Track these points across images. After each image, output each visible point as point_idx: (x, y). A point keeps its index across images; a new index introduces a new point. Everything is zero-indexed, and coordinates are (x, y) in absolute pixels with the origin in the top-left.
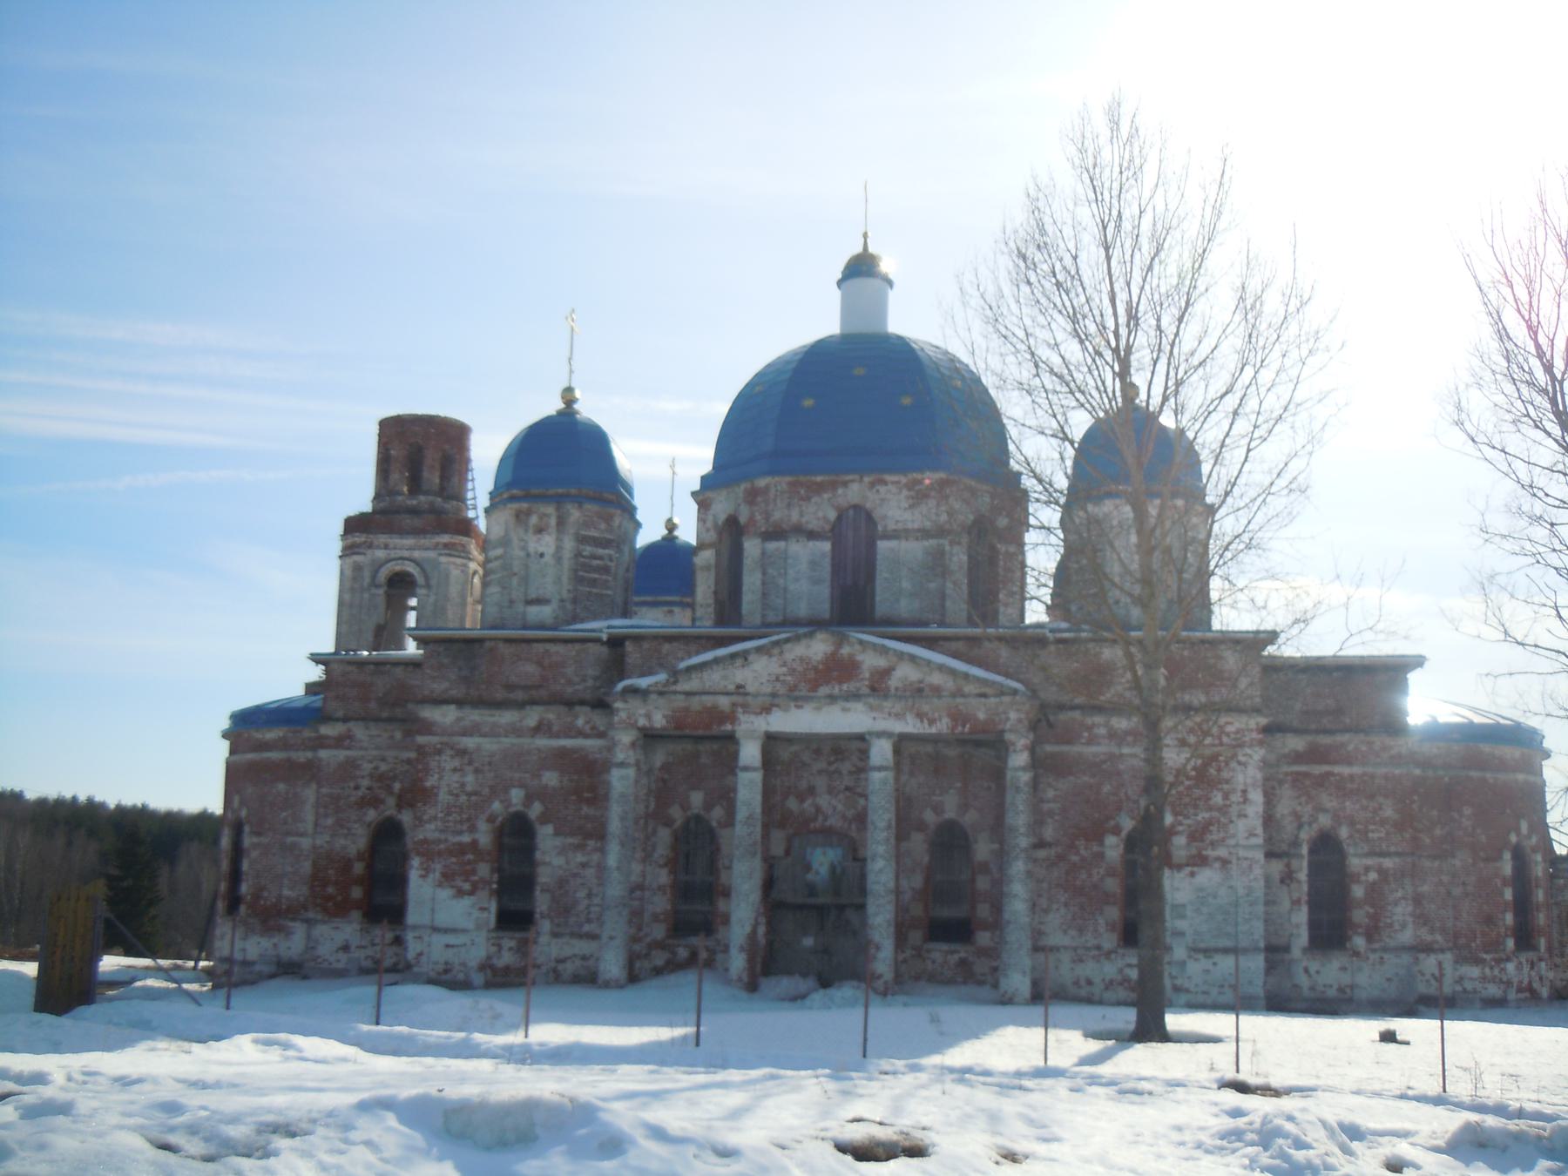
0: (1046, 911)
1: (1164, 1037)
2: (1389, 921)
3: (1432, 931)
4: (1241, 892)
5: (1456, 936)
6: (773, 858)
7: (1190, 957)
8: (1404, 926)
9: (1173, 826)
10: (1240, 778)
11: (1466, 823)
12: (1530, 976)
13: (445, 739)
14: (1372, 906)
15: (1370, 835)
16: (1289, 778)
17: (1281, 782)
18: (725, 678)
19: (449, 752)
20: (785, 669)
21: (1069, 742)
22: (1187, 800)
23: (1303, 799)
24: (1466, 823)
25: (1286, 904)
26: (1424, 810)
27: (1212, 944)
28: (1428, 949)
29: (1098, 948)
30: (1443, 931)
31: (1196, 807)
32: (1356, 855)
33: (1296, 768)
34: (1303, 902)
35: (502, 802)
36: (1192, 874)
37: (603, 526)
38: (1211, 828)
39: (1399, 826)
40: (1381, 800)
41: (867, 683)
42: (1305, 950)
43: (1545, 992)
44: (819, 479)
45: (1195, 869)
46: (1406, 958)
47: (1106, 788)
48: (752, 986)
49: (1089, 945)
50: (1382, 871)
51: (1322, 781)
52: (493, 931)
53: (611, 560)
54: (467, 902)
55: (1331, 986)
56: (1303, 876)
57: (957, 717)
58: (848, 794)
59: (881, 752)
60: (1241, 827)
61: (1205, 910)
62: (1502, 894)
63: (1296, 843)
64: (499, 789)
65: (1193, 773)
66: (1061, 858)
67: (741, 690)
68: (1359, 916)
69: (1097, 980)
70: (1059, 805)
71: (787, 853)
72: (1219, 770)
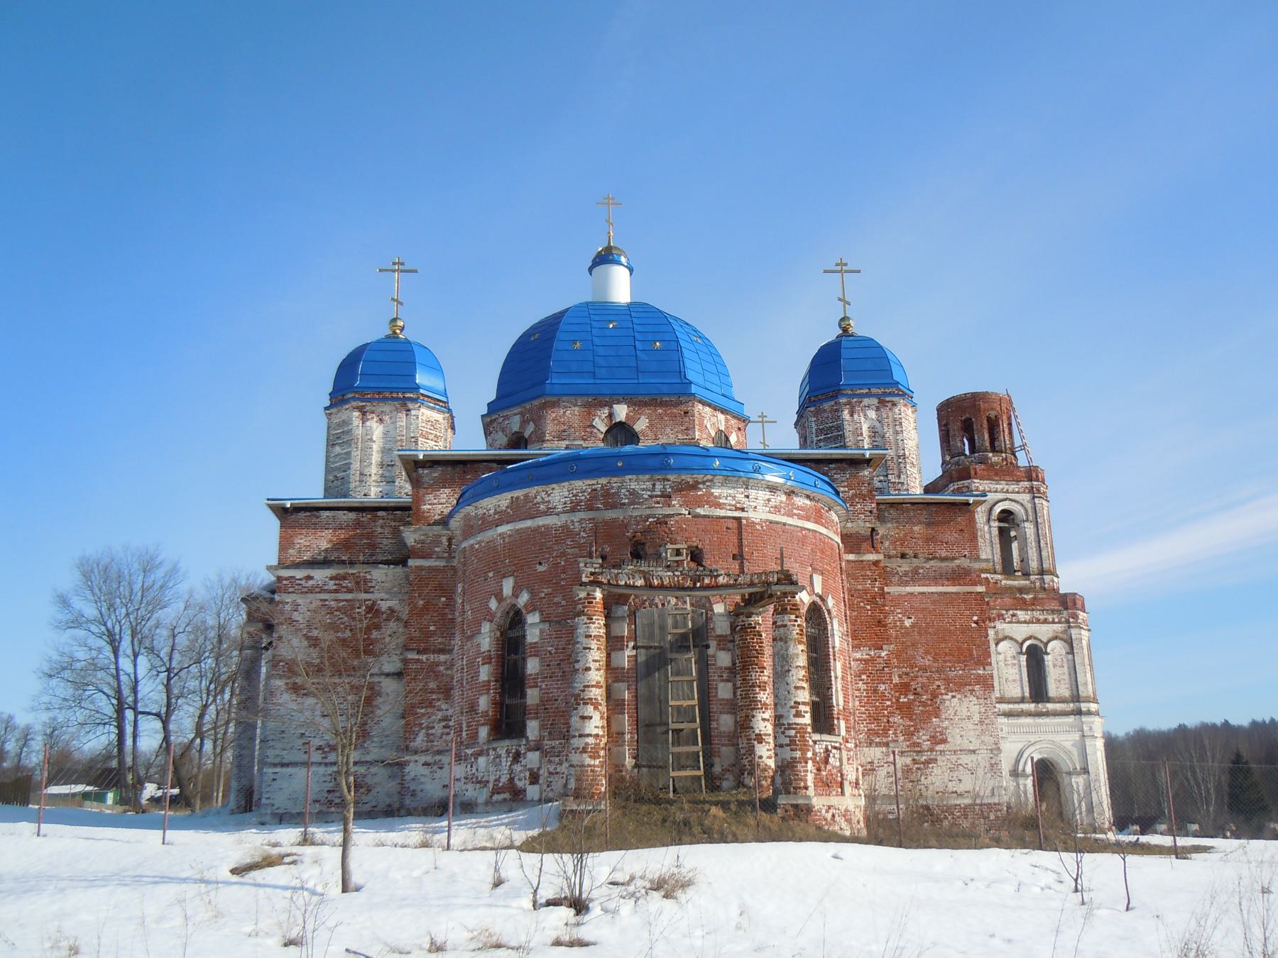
12: (511, 771)
43: (533, 792)
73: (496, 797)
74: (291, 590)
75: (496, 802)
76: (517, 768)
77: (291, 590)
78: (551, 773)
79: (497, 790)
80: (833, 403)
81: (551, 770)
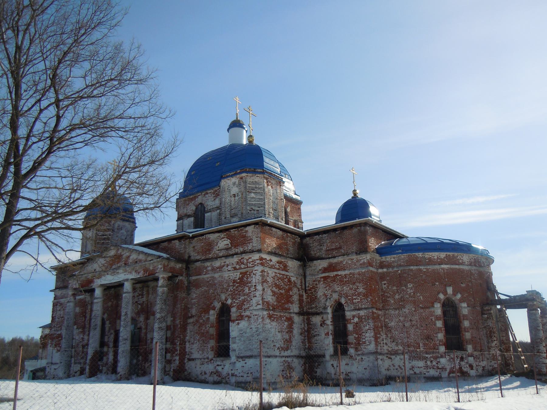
0: (193, 344)
2: (364, 340)
3: (397, 344)
4: (254, 330)
7: (237, 360)
8: (370, 343)
9: (232, 303)
10: (254, 281)
14: (357, 334)
15: (354, 301)
16: (322, 279)
17: (319, 281)
18: (92, 267)
20: (105, 261)
21: (200, 275)
22: (236, 292)
23: (328, 288)
24: (409, 291)
25: (323, 335)
26: (390, 287)
28: (396, 353)
29: (208, 358)
30: (403, 344)
32: (348, 311)
34: (330, 334)
36: (238, 324)
37: (107, 225)
38: (245, 303)
39: (366, 296)
40: (358, 284)
41: (124, 262)
42: (331, 356)
43: (473, 373)
44: (191, 197)
45: (239, 321)
46: (372, 358)
47: (211, 291)
48: (90, 377)
50: (359, 317)
51: (334, 279)
53: (110, 235)
56: (329, 322)
57: (146, 270)
58: (136, 304)
59: (128, 286)
60: (254, 301)
61: (242, 339)
62: (435, 324)
63: (325, 308)
65: (239, 281)
66: (197, 321)
68: (351, 338)
69: (207, 372)
70: (197, 300)
72: (247, 278)
73: (451, 375)
74: (266, 265)
75: (452, 377)
76: (463, 363)
77: (266, 265)
78: (477, 365)
79: (452, 372)
81: (477, 364)
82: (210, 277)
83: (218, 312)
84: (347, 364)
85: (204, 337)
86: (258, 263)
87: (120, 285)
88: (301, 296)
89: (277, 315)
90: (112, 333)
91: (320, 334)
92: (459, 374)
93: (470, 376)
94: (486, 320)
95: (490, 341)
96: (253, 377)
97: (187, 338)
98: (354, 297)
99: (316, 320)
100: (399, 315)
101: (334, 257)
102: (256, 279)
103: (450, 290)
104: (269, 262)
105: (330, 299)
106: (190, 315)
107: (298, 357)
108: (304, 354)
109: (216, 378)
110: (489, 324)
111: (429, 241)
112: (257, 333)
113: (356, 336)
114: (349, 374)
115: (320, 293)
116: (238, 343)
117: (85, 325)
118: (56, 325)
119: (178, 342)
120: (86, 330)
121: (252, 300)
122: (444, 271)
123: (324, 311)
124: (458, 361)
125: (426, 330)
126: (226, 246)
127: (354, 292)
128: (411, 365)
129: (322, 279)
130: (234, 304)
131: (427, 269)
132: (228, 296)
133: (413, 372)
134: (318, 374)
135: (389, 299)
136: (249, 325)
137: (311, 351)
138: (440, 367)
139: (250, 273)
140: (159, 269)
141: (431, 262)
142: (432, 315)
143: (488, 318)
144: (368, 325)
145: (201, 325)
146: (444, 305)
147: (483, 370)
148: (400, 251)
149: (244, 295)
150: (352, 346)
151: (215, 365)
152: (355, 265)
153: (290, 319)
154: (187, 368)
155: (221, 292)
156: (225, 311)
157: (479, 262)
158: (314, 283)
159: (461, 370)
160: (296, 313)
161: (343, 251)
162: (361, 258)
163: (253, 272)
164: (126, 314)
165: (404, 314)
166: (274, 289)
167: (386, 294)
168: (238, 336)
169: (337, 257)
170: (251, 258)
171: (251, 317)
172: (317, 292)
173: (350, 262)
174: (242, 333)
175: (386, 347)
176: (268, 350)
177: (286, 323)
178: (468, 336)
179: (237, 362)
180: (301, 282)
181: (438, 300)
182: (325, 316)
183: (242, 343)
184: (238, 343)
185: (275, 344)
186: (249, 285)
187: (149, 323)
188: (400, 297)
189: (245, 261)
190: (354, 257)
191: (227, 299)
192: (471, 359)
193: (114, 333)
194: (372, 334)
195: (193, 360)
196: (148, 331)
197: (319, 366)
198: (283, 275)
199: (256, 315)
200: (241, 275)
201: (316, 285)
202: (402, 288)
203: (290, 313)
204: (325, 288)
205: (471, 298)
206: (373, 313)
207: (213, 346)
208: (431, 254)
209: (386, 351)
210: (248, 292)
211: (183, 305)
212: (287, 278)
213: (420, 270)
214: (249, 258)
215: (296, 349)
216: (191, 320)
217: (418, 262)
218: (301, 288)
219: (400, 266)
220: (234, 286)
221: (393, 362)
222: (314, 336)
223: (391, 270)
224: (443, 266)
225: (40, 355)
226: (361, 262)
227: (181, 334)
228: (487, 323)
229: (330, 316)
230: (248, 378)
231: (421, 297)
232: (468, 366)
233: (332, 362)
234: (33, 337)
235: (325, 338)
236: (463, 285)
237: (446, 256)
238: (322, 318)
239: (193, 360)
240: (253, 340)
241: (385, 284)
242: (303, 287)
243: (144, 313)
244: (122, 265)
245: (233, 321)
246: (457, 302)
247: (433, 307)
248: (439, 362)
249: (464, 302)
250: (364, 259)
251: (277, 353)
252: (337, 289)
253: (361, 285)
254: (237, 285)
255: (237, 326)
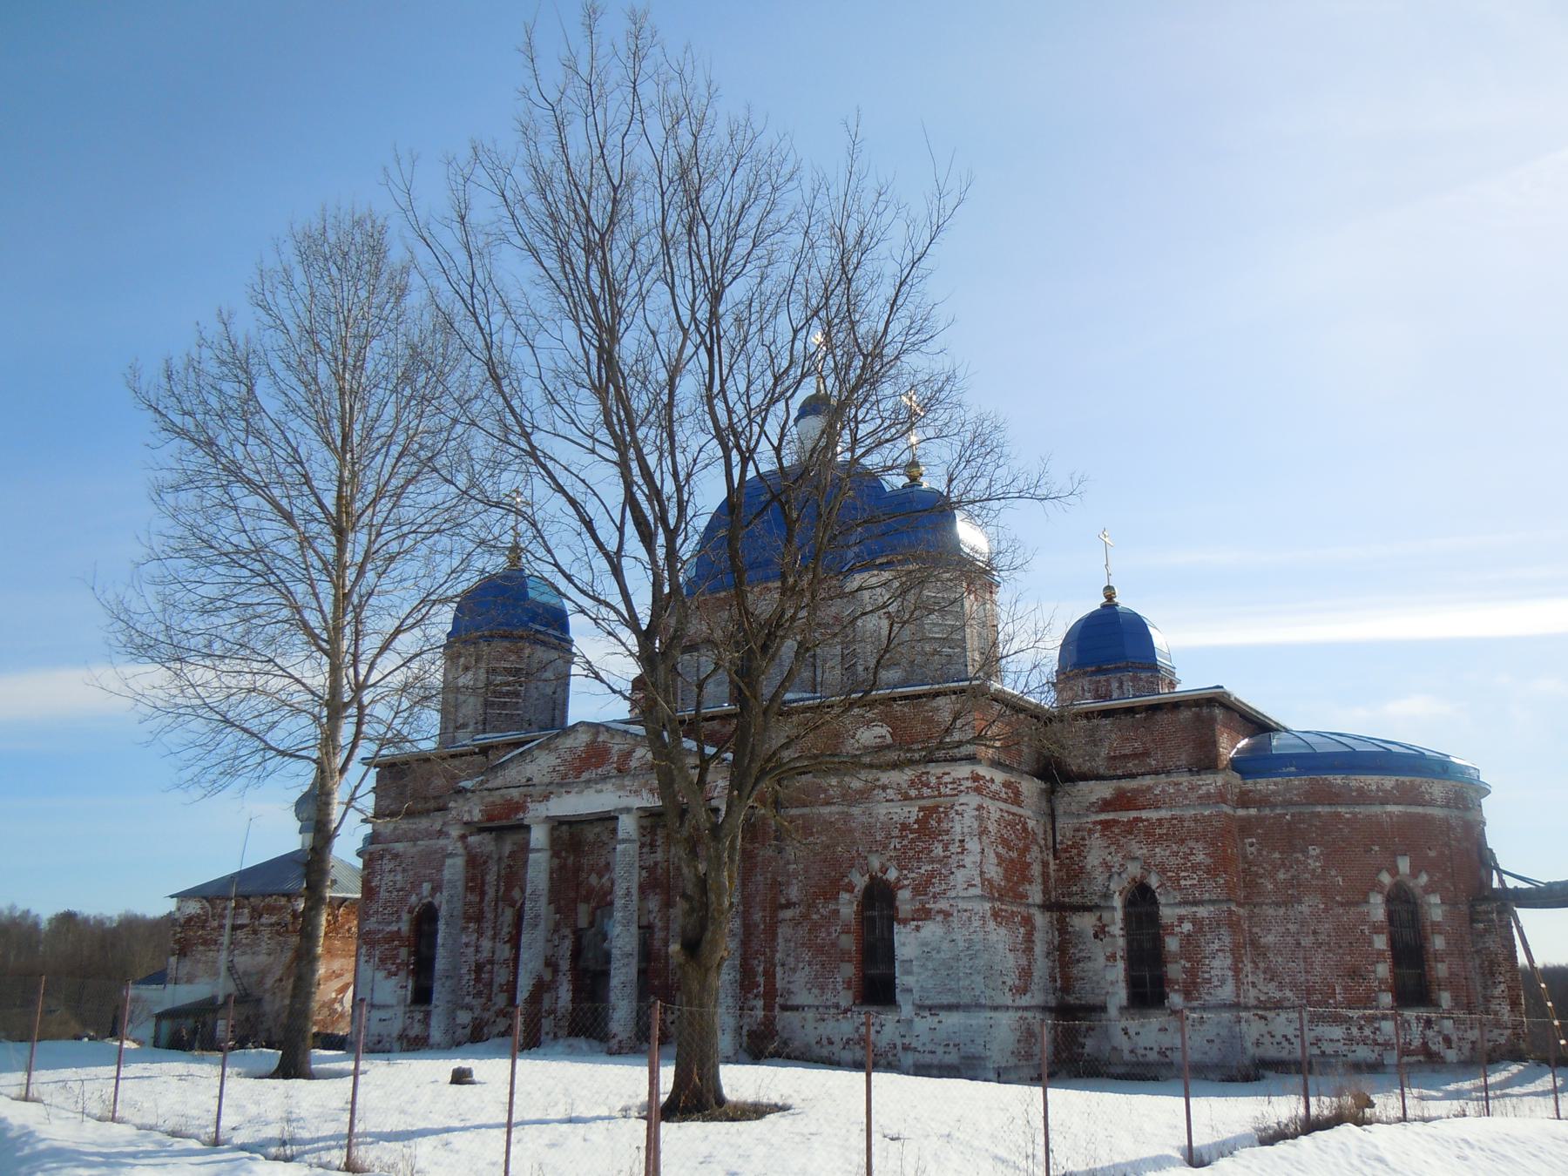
0: (794, 970)
1: (310, 1076)
2: (1206, 976)
3: (1281, 987)
4: (962, 945)
5: (1309, 991)
6: (581, 929)
8: (1223, 982)
9: (898, 879)
10: (958, 828)
11: (1314, 864)
12: (1424, 1036)
13: (384, 846)
15: (1183, 882)
17: (1091, 832)
19: (389, 857)
20: (559, 760)
22: (911, 853)
23: (1113, 848)
24: (1312, 864)
25: (1102, 960)
27: (936, 1001)
28: (1278, 1006)
29: (837, 1006)
30: (1294, 986)
31: (919, 860)
33: (1103, 817)
34: (1118, 957)
35: (417, 895)
36: (918, 928)
38: (934, 880)
39: (1212, 872)
40: (1192, 844)
42: (1122, 1009)
43: (1451, 1055)
45: (920, 923)
46: (1227, 1016)
49: (829, 1003)
50: (1195, 921)
52: (409, 1006)
54: (394, 981)
55: (1151, 1049)
56: (1117, 929)
59: (628, 826)
60: (960, 877)
61: (930, 965)
62: (1371, 943)
63: (1107, 896)
64: (416, 886)
65: (916, 826)
66: (805, 917)
67: (530, 783)
68: (1175, 971)
69: (836, 1039)
71: (592, 924)
72: (939, 821)
76: (1430, 1033)
80: (1149, 674)
82: (838, 813)
83: (860, 898)
84: (1163, 1030)
85: (826, 955)
86: (967, 788)
87: (608, 819)
88: (1045, 864)
89: (1006, 911)
90: (566, 936)
91: (1093, 957)
92: (1421, 1058)
93: (1445, 1062)
94: (1482, 936)
95: (1490, 983)
96: (962, 1054)
97: (778, 955)
98: (1183, 874)
99: (1084, 923)
100: (1286, 919)
101: (1132, 776)
102: (962, 824)
103: (1404, 865)
104: (989, 784)
105: (1119, 874)
106: (783, 901)
107: (1045, 1009)
108: (1053, 1003)
109: (859, 1054)
110: (1487, 945)
111: (1361, 747)
112: (970, 952)
113: (1188, 965)
114: (1168, 1053)
115: (1093, 859)
116: (919, 974)
117: (482, 912)
118: (381, 909)
119: (759, 966)
120: (485, 925)
121: (952, 873)
122: (1391, 819)
123: (1103, 904)
124: (1420, 1029)
125: (1349, 954)
126: (878, 740)
127: (1182, 861)
128: (1313, 1034)
129: (1099, 827)
130: (906, 882)
131: (1355, 815)
132: (888, 860)
133: (1318, 1052)
134: (1087, 1050)
135: (1262, 880)
136: (948, 932)
137: (1068, 994)
138: (1379, 1041)
139: (945, 808)
140: (718, 789)
141: (1363, 797)
142: (1364, 922)
143: (1486, 930)
144: (1217, 941)
145: (815, 927)
146: (1389, 900)
147: (1473, 1049)
148: (1293, 769)
149: (933, 862)
150: (1176, 987)
151: (856, 1024)
152: (1186, 797)
153: (1028, 921)
154: (778, 1028)
155: (869, 852)
156: (879, 897)
157: (1464, 799)
158: (1077, 834)
159: (1425, 1048)
160: (1039, 906)
161: (1153, 763)
162: (1201, 783)
163: (956, 808)
164: (628, 894)
165: (1299, 916)
166: (1000, 849)
167: (1255, 868)
168: (917, 958)
169: (1139, 778)
170: (949, 774)
171: (952, 915)
172: (1085, 858)
173: (1172, 791)
174: (928, 951)
175: (1252, 993)
176: (993, 993)
177: (1022, 930)
178: (1441, 970)
179: (917, 1019)
180: (1045, 832)
181: (1377, 886)
182: (1106, 916)
183: (930, 973)
184: (919, 974)
185: (1006, 979)
186: (946, 837)
187: (672, 917)
188: (1288, 876)
189: (933, 780)
190: (1185, 780)
191: (887, 870)
192: (1448, 1024)
193: (571, 936)
194: (1229, 962)
195: (796, 1008)
196: (671, 934)
197: (1091, 1032)
198: (1014, 814)
199: (966, 911)
200: (922, 814)
201: (1083, 839)
202: (1295, 855)
203: (1029, 905)
204: (1105, 847)
205: (1448, 884)
206: (1230, 912)
207: (850, 978)
208: (1362, 778)
209: (1253, 1002)
210: (942, 854)
211: (769, 875)
212: (1020, 821)
213: (1338, 815)
214: (944, 774)
215: (1039, 990)
216: (788, 914)
217: (1333, 797)
218: (1046, 845)
219: (1291, 803)
220: (903, 838)
221: (1271, 1027)
222: (1078, 961)
223: (1267, 811)
224: (1389, 808)
225: (171, 972)
226: (1200, 792)
227: (765, 947)
228: (1484, 943)
229: (1119, 915)
230: (947, 1056)
231: (1340, 879)
232: (1441, 1039)
233: (1123, 1023)
234: (28, 911)
235: (1106, 966)
236: (1432, 854)
237: (1397, 786)
238: (1100, 919)
239: (796, 1008)
240: (958, 968)
241: (1252, 845)
242: (1050, 843)
243: (658, 890)
244: (609, 772)
245: (905, 922)
246: (1418, 892)
247: (1367, 902)
248: (1378, 1029)
249: (1433, 892)
250: (1207, 785)
251: (1008, 999)
252: (1138, 853)
253: (1200, 846)
254: (911, 836)
255: (913, 934)
